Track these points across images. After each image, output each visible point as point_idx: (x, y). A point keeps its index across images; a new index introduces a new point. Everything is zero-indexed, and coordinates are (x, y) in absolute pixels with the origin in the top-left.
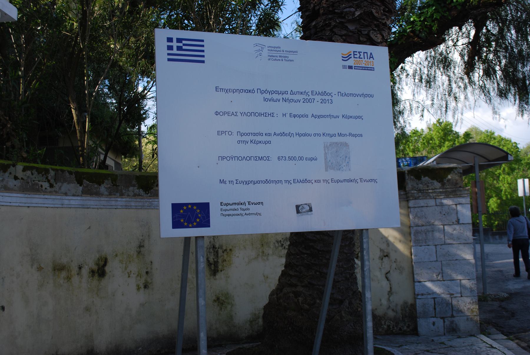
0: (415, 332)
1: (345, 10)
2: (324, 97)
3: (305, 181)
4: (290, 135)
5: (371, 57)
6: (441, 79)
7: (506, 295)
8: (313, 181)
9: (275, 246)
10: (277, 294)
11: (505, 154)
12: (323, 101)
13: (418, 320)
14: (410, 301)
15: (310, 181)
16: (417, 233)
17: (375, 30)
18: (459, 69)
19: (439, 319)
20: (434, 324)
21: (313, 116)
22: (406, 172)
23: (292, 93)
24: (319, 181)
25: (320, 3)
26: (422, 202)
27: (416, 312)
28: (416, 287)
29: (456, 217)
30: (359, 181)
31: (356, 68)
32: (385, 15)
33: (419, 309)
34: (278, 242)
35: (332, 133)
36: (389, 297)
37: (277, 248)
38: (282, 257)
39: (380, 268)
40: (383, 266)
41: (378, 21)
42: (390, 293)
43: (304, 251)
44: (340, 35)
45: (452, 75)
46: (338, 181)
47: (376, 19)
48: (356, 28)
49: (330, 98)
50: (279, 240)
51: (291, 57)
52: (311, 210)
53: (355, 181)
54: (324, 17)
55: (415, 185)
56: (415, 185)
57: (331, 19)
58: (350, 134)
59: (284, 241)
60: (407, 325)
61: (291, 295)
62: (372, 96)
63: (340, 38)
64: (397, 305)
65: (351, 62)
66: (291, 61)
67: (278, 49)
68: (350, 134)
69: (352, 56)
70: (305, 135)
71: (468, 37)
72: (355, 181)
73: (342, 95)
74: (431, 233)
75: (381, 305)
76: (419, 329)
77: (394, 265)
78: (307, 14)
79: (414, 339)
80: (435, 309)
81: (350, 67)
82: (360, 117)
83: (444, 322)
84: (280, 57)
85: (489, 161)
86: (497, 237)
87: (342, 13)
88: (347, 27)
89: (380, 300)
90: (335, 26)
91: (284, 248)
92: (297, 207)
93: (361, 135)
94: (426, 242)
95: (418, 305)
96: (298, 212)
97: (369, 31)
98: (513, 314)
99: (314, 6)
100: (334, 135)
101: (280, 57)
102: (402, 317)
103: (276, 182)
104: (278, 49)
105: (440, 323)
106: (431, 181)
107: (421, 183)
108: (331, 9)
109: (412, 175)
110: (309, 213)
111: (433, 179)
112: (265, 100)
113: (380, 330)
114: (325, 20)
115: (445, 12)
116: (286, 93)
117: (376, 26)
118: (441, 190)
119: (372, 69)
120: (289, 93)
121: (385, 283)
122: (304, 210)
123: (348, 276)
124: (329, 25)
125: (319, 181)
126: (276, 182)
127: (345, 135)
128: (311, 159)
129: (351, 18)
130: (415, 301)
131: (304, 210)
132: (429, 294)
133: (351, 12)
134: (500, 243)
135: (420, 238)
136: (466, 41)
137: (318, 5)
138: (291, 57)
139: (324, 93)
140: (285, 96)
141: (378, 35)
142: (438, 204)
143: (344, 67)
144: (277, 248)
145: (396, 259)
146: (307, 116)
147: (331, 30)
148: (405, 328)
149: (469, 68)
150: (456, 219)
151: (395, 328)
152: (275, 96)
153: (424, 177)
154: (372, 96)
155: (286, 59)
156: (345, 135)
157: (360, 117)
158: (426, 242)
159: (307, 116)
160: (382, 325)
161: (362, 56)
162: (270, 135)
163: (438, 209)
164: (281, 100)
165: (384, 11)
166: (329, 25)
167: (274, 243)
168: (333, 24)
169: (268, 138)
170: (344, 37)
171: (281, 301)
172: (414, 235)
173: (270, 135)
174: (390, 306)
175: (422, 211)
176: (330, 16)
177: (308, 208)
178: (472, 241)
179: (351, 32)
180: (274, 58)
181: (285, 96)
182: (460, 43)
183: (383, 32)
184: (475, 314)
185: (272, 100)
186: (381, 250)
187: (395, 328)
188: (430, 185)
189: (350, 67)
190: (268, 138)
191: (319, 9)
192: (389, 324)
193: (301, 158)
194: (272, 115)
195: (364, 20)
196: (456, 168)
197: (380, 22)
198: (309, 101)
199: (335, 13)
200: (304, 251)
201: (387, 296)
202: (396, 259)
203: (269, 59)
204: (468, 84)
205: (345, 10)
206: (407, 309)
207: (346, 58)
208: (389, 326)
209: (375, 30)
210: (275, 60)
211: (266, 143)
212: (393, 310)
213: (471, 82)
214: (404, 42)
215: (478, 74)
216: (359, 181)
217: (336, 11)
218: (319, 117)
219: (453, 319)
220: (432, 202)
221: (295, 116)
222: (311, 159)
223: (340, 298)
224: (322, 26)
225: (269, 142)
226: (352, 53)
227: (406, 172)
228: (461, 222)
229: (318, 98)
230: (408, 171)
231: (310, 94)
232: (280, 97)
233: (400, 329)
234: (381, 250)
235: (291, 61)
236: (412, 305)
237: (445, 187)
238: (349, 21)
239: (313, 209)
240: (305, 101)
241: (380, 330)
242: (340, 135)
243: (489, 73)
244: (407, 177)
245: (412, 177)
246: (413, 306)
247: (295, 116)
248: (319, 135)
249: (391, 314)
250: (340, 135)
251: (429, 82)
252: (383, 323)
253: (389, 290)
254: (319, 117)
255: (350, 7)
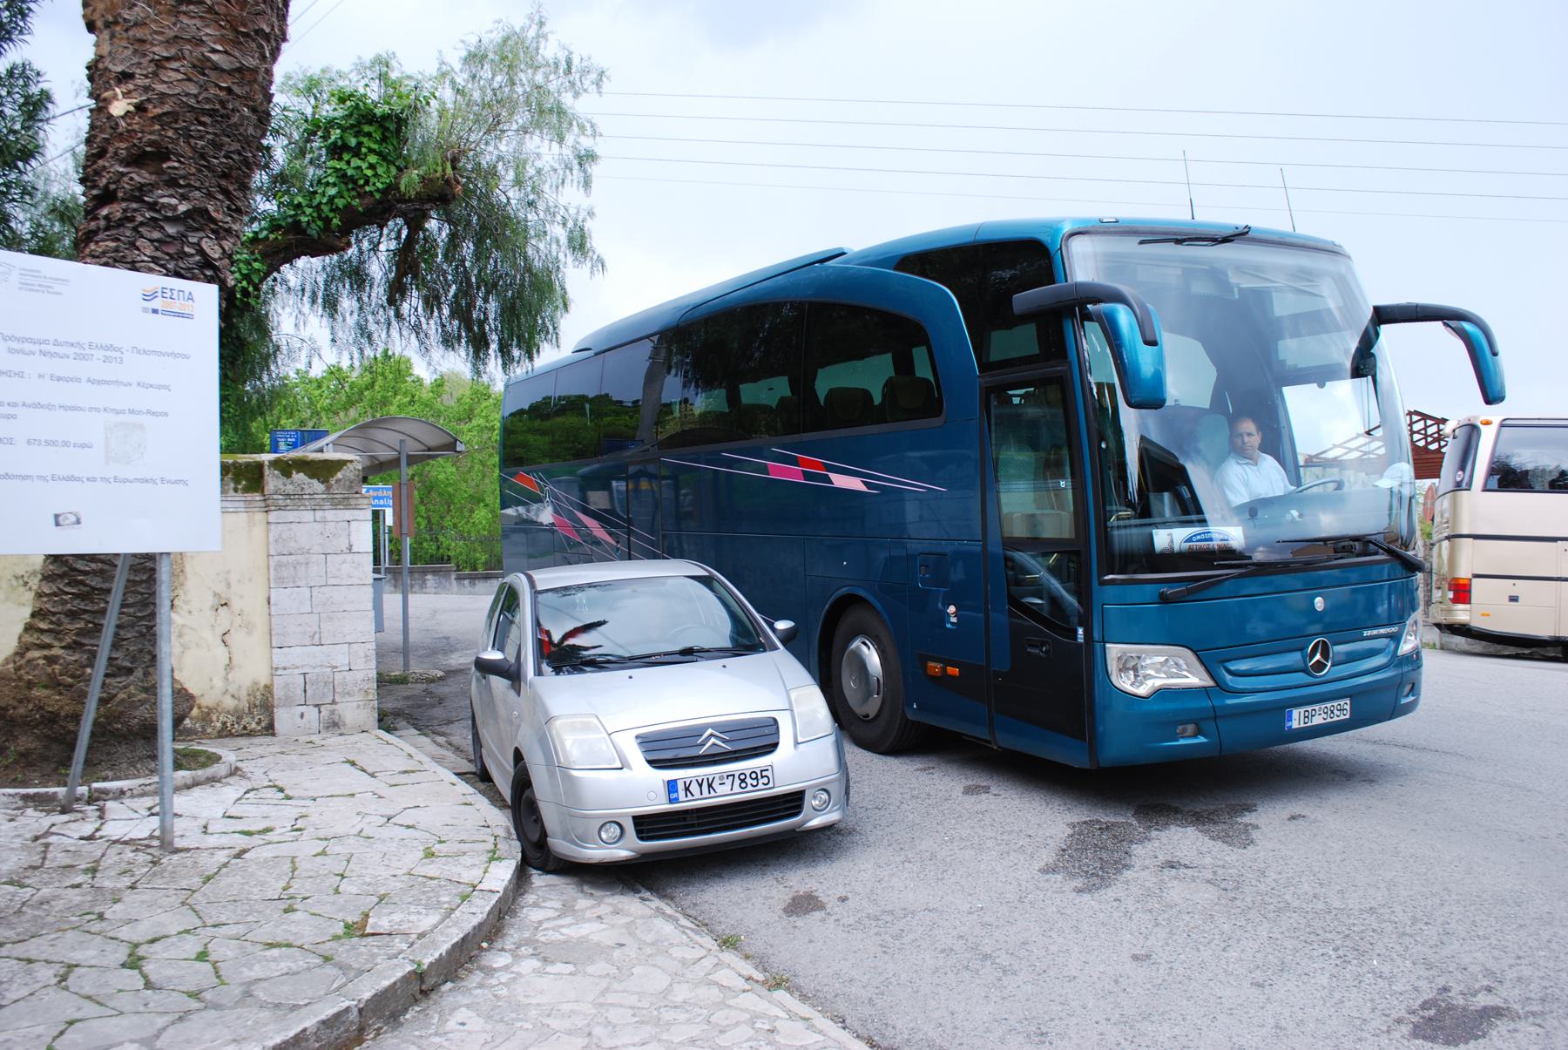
0: (270, 730)
1: (162, 200)
2: (108, 353)
3: (72, 478)
4: (49, 407)
5: (191, 298)
6: (347, 303)
7: (440, 674)
8: (84, 479)
9: (11, 585)
10: (15, 662)
11: (452, 440)
12: (107, 360)
13: (275, 710)
14: (264, 680)
15: (78, 479)
16: (279, 565)
17: (211, 238)
18: (378, 293)
19: (311, 707)
20: (302, 716)
21: (89, 380)
22: (267, 463)
23: (57, 343)
24: (93, 480)
25: (118, 181)
26: (291, 516)
27: (273, 697)
28: (274, 656)
29: (347, 542)
30: (159, 481)
31: (165, 313)
32: (231, 216)
33: (278, 692)
34: (16, 578)
35: (119, 408)
36: (227, 674)
37: (14, 588)
38: (24, 605)
39: (212, 626)
40: (219, 622)
41: (217, 225)
42: (229, 666)
43: (67, 589)
44: (149, 240)
45: (366, 299)
46: (125, 481)
47: (214, 221)
48: (178, 232)
49: (118, 354)
50: (21, 574)
51: (57, 288)
52: (78, 522)
53: (153, 481)
54: (124, 205)
55: (281, 486)
56: (281, 486)
57: (135, 210)
58: (149, 412)
59: (29, 577)
60: (256, 720)
61: (42, 662)
62: (186, 357)
63: (149, 243)
64: (240, 687)
65: (157, 303)
66: (58, 293)
67: (37, 274)
68: (149, 412)
69: (159, 294)
70: (74, 408)
71: (398, 237)
72: (153, 481)
73: (139, 352)
74: (303, 567)
75: (212, 688)
76: (277, 725)
77: (238, 620)
78: (95, 192)
79: (268, 739)
80: (305, 691)
81: (155, 311)
82: (166, 387)
83: (320, 712)
84: (39, 286)
85: (429, 450)
86: (467, 582)
87: (156, 203)
88: (163, 228)
89: (211, 680)
90: (142, 224)
91: (30, 589)
92: (57, 516)
93: (166, 414)
94: (294, 582)
95: (275, 686)
96: (57, 524)
97: (201, 238)
98: (441, 701)
99: (109, 183)
100: (122, 412)
101: (39, 286)
102: (249, 708)
103: (25, 478)
104: (37, 274)
105: (311, 713)
106: (310, 480)
107: (292, 483)
108: (137, 194)
109: (275, 469)
110: (76, 526)
111: (311, 477)
112: (10, 350)
113: (209, 730)
114: (125, 211)
115: (353, 198)
116: (46, 342)
117: (213, 231)
118: (324, 496)
119: (189, 316)
120: (51, 342)
121: (221, 651)
122: (67, 522)
123: (144, 630)
124: (132, 219)
125: (93, 480)
126: (25, 478)
127: (140, 412)
128: (83, 446)
129: (170, 214)
130: (272, 680)
131: (67, 522)
132: (297, 667)
133: (170, 205)
134: (470, 593)
135: (285, 574)
136: (393, 245)
137: (114, 183)
138: (57, 288)
139: (110, 347)
140: (44, 347)
141: (216, 247)
142: (318, 519)
143: (145, 310)
144: (14, 588)
145: (241, 610)
146: (78, 380)
147: (135, 229)
148: (253, 725)
149: (396, 291)
150: (347, 546)
151: (236, 726)
152: (27, 347)
153: (298, 472)
154: (186, 357)
155: (51, 290)
156: (140, 412)
157: (166, 387)
158: (294, 582)
159: (78, 380)
160: (212, 722)
161: (175, 296)
162: (15, 405)
163: (318, 527)
164: (38, 352)
165: (229, 208)
166: (132, 219)
167: (10, 580)
168: (140, 219)
169: (11, 410)
170: (156, 244)
171: (23, 672)
172: (275, 570)
173: (15, 405)
174: (227, 690)
175: (290, 530)
176: (135, 205)
177: (73, 519)
178: (372, 581)
179: (169, 236)
180: (29, 287)
181: (44, 347)
182: (382, 247)
183: (225, 242)
184: (371, 697)
185: (22, 352)
186: (216, 594)
187: (236, 726)
188: (306, 487)
189: (155, 311)
190: (11, 410)
191: (115, 190)
192: (225, 719)
193: (66, 444)
194: (20, 375)
195: (194, 220)
196: (351, 461)
197: (221, 227)
198: (84, 357)
199: (144, 201)
200: (67, 589)
201: (224, 673)
202: (241, 610)
203: (21, 289)
204: (393, 319)
205: (162, 200)
206: (258, 693)
207: (148, 297)
208: (224, 723)
209: (211, 238)
210: (32, 290)
211: (9, 417)
212: (233, 696)
213: (398, 316)
214: (280, 238)
215: (412, 303)
216: (159, 481)
217: (146, 199)
218: (99, 382)
219: (334, 707)
220: (308, 516)
221: (59, 379)
222: (83, 446)
223: (129, 665)
224: (120, 219)
225: (14, 417)
226: (160, 291)
227: (267, 463)
228: (354, 549)
229: (100, 354)
230: (269, 462)
231: (86, 346)
232: (36, 348)
233: (245, 728)
234: (216, 594)
235: (58, 293)
236: (266, 686)
237: (332, 491)
238: (167, 219)
239: (82, 521)
240: (77, 357)
241: (209, 730)
242: (132, 412)
243: (432, 302)
244: (267, 471)
245: (276, 472)
246: (269, 688)
247: (59, 379)
248: (97, 410)
249: (229, 703)
250: (132, 412)
251: (331, 305)
252: (214, 718)
253: (227, 662)
254: (99, 382)
255: (171, 196)
